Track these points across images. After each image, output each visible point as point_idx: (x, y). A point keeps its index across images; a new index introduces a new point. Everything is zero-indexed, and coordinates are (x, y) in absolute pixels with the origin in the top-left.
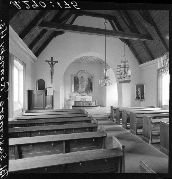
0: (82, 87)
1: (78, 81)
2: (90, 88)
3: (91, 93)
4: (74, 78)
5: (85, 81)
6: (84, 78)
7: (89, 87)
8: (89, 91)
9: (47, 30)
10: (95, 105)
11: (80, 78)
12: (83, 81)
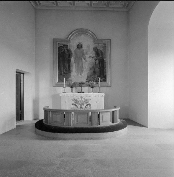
0: (80, 70)
1: (70, 56)
2: (99, 73)
3: (102, 86)
4: (60, 49)
5: (87, 56)
6: (84, 48)
7: (97, 70)
8: (97, 82)
9: (71, 5)
10: (110, 124)
11: (73, 46)
12: (83, 56)
